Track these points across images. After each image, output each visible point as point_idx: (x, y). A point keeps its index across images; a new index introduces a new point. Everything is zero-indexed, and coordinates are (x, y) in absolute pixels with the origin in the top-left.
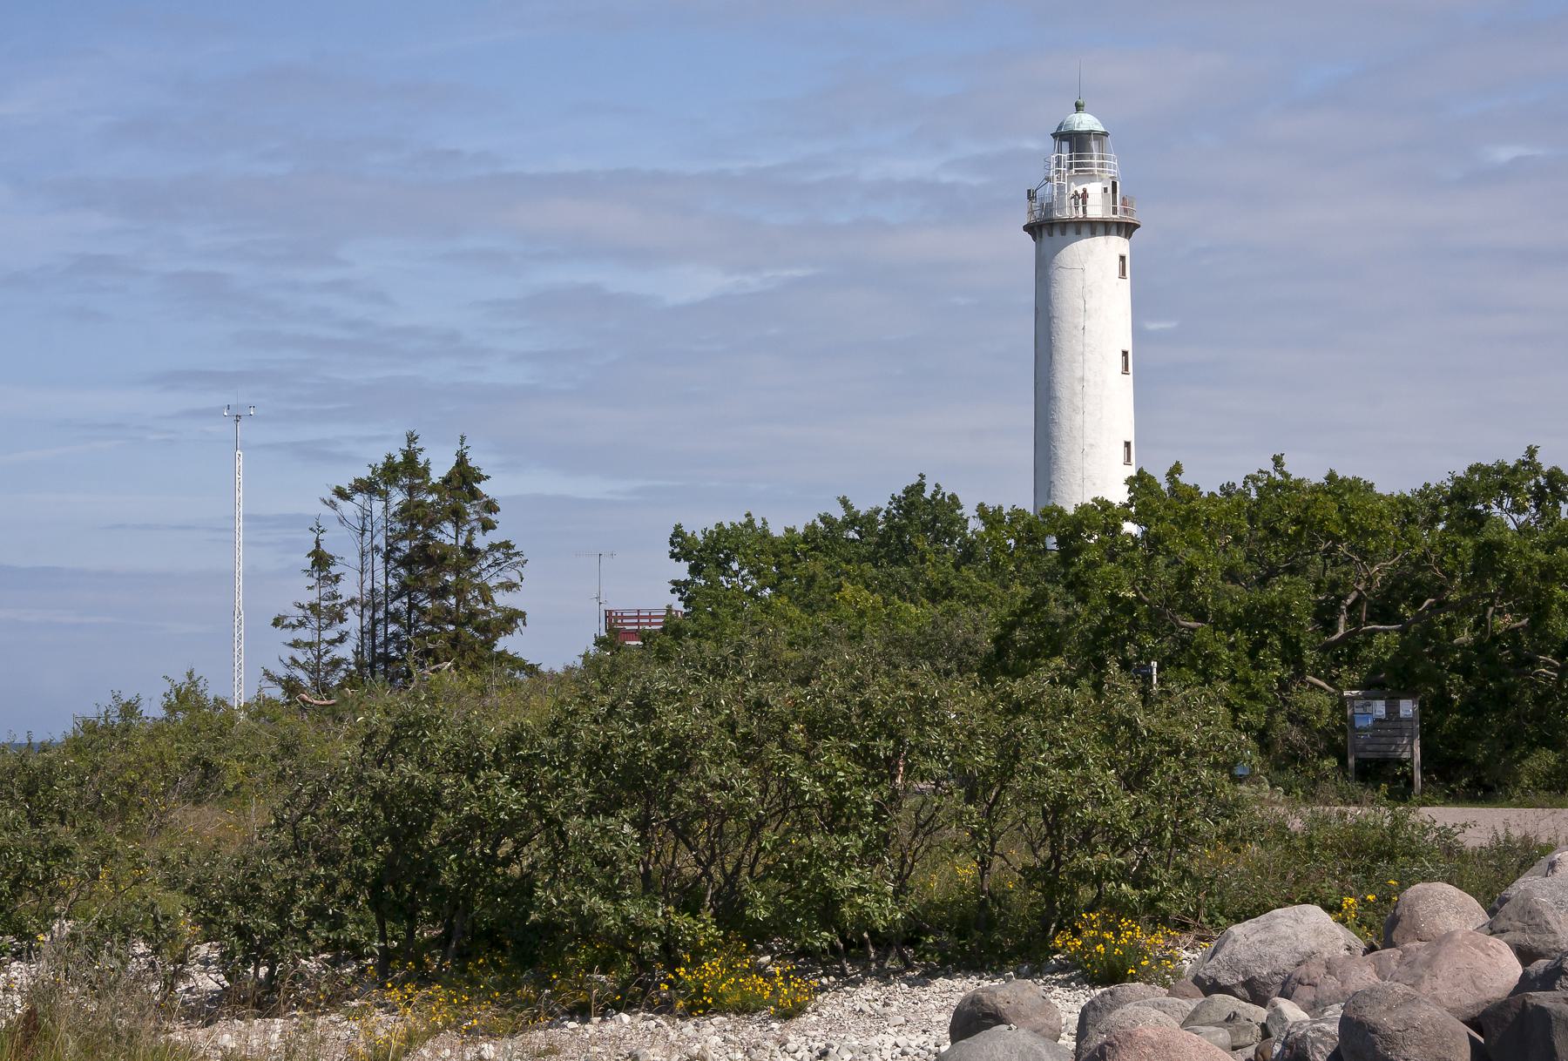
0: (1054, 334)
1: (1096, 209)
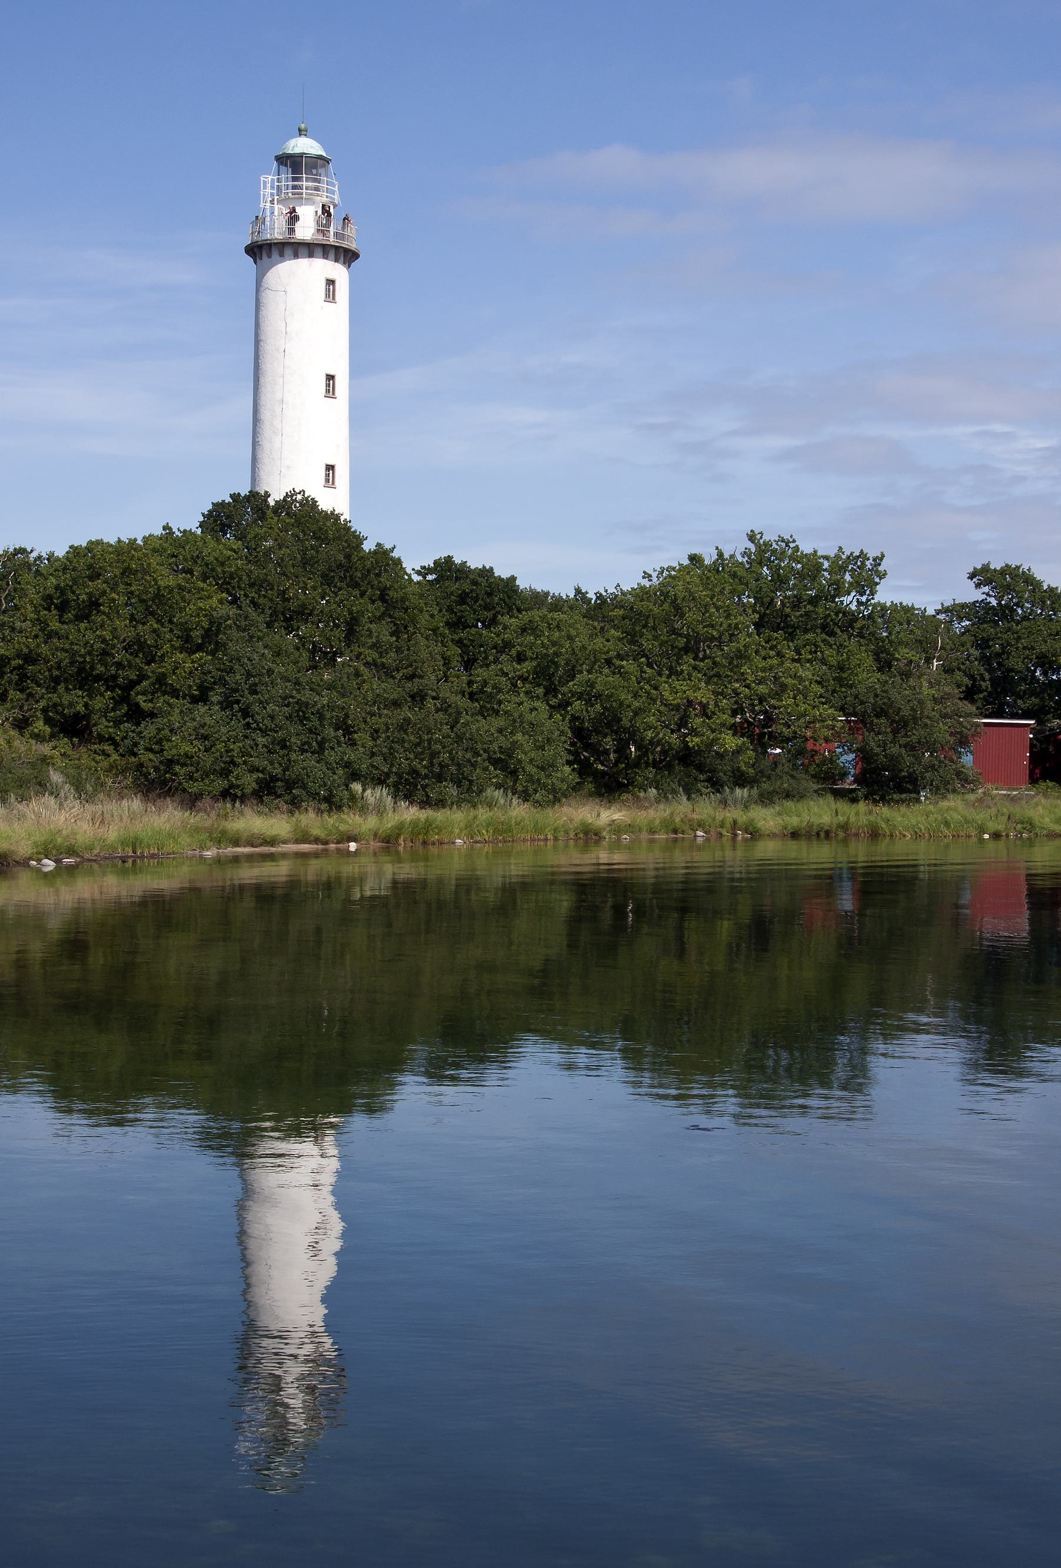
1: (306, 230)
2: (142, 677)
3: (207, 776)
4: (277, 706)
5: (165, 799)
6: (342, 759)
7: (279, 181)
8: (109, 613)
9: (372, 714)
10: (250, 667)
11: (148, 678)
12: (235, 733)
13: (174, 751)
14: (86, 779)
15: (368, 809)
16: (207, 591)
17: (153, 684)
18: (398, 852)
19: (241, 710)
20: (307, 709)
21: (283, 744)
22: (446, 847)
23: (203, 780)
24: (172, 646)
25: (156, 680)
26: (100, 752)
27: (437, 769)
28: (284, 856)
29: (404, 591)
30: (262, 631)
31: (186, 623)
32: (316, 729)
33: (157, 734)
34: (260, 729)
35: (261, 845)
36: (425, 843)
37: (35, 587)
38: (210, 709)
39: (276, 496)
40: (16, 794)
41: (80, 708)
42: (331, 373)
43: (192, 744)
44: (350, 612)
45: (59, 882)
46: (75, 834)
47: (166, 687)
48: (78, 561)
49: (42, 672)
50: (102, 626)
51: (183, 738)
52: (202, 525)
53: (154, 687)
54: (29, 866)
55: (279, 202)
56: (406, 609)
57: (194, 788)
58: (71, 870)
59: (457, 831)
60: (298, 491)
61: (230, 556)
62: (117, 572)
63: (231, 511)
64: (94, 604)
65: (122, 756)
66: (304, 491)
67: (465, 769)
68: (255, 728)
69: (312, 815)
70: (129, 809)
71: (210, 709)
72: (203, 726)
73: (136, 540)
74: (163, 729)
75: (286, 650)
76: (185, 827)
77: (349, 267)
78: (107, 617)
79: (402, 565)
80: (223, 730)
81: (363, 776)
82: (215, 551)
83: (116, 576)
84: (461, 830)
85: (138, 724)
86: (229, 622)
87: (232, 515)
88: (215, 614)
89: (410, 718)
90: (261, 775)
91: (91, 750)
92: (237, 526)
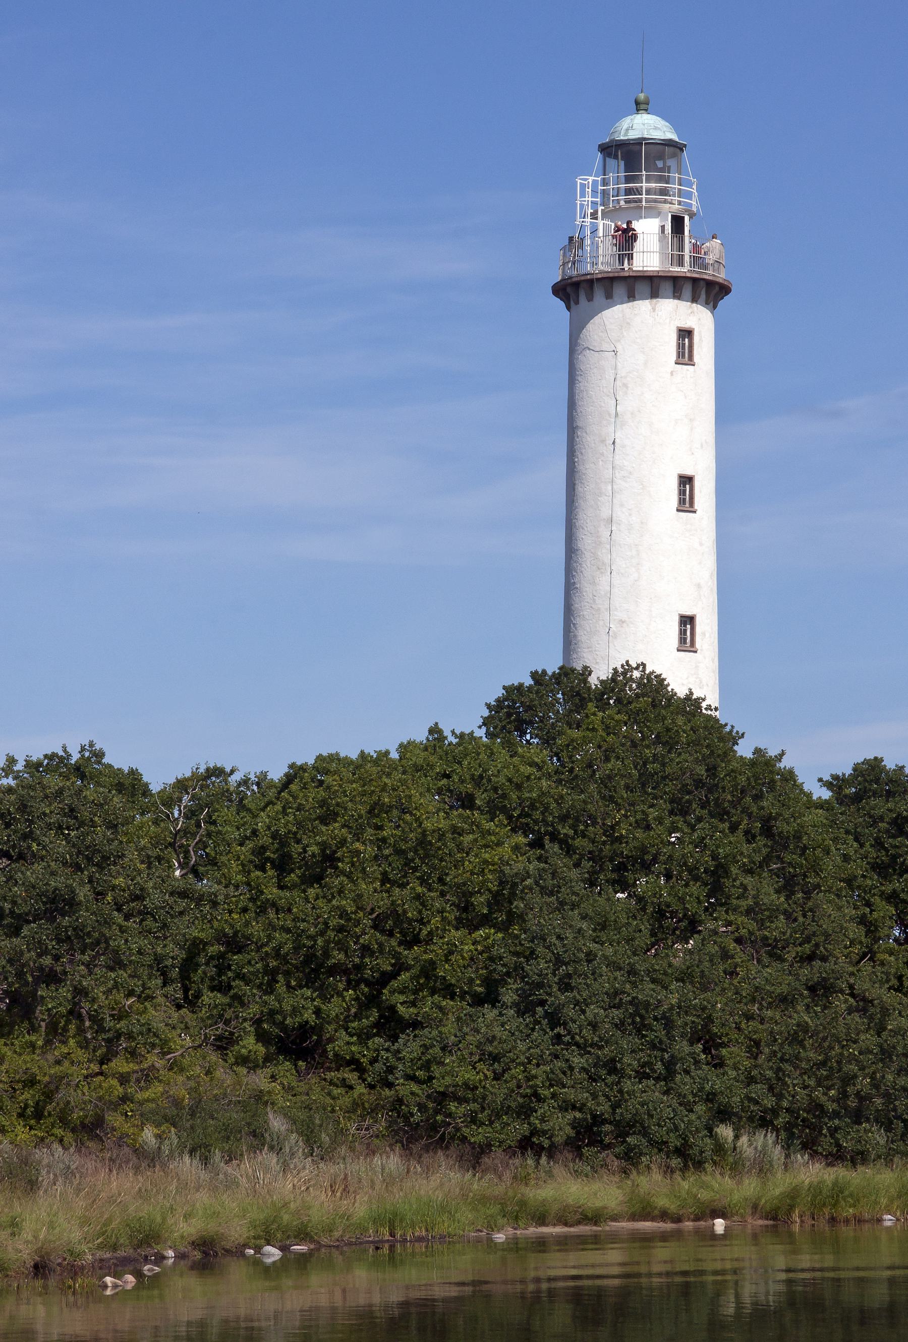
0: (578, 453)
2: (400, 967)
3: (498, 1116)
4: (602, 1007)
5: (436, 1153)
6: (701, 1089)
7: (605, 183)
8: (351, 872)
9: (749, 1017)
10: (561, 950)
11: (408, 968)
12: (538, 1051)
13: (448, 1080)
14: (321, 1126)
15: (743, 1165)
16: (495, 834)
17: (416, 978)
18: (791, 1235)
19: (546, 1014)
20: (647, 1012)
21: (612, 1066)
22: (867, 1226)
23: (491, 1123)
24: (444, 919)
25: (421, 971)
26: (338, 1082)
27: (852, 1103)
28: (614, 1238)
29: (799, 821)
30: (578, 895)
31: (464, 884)
32: (661, 1042)
33: (423, 1053)
34: (577, 1045)
35: (579, 1223)
36: (833, 1220)
37: (238, 829)
38: (501, 1014)
39: (600, 673)
40: (222, 1151)
41: (309, 1016)
42: (688, 472)
43: (475, 1068)
44: (714, 857)
45: (287, 1282)
46: (309, 1208)
47: (435, 982)
48: (305, 796)
49: (253, 962)
50: (340, 892)
51: (462, 1059)
52: (486, 722)
53: (418, 982)
54: (243, 1255)
55: (605, 215)
56: (805, 848)
57: (478, 1135)
58: (303, 1261)
59: (884, 1201)
60: (634, 665)
61: (531, 774)
62: (363, 809)
63: (532, 701)
64: (329, 859)
65: (371, 1087)
66: (644, 665)
67: (897, 1103)
68: (568, 1044)
69: (657, 1176)
70: (383, 1169)
71: (501, 1014)
72: (491, 1040)
73: (387, 753)
74: (432, 1046)
75: (616, 921)
76: (464, 1196)
77: (715, 307)
78: (348, 877)
79: (795, 781)
80: (521, 1046)
81: (736, 1114)
82: (508, 768)
83: (360, 816)
84: (891, 1201)
85: (394, 1038)
86: (529, 882)
87: (534, 706)
88: (507, 869)
89: (807, 1023)
90: (578, 1115)
91: (325, 1079)
92: (541, 721)
